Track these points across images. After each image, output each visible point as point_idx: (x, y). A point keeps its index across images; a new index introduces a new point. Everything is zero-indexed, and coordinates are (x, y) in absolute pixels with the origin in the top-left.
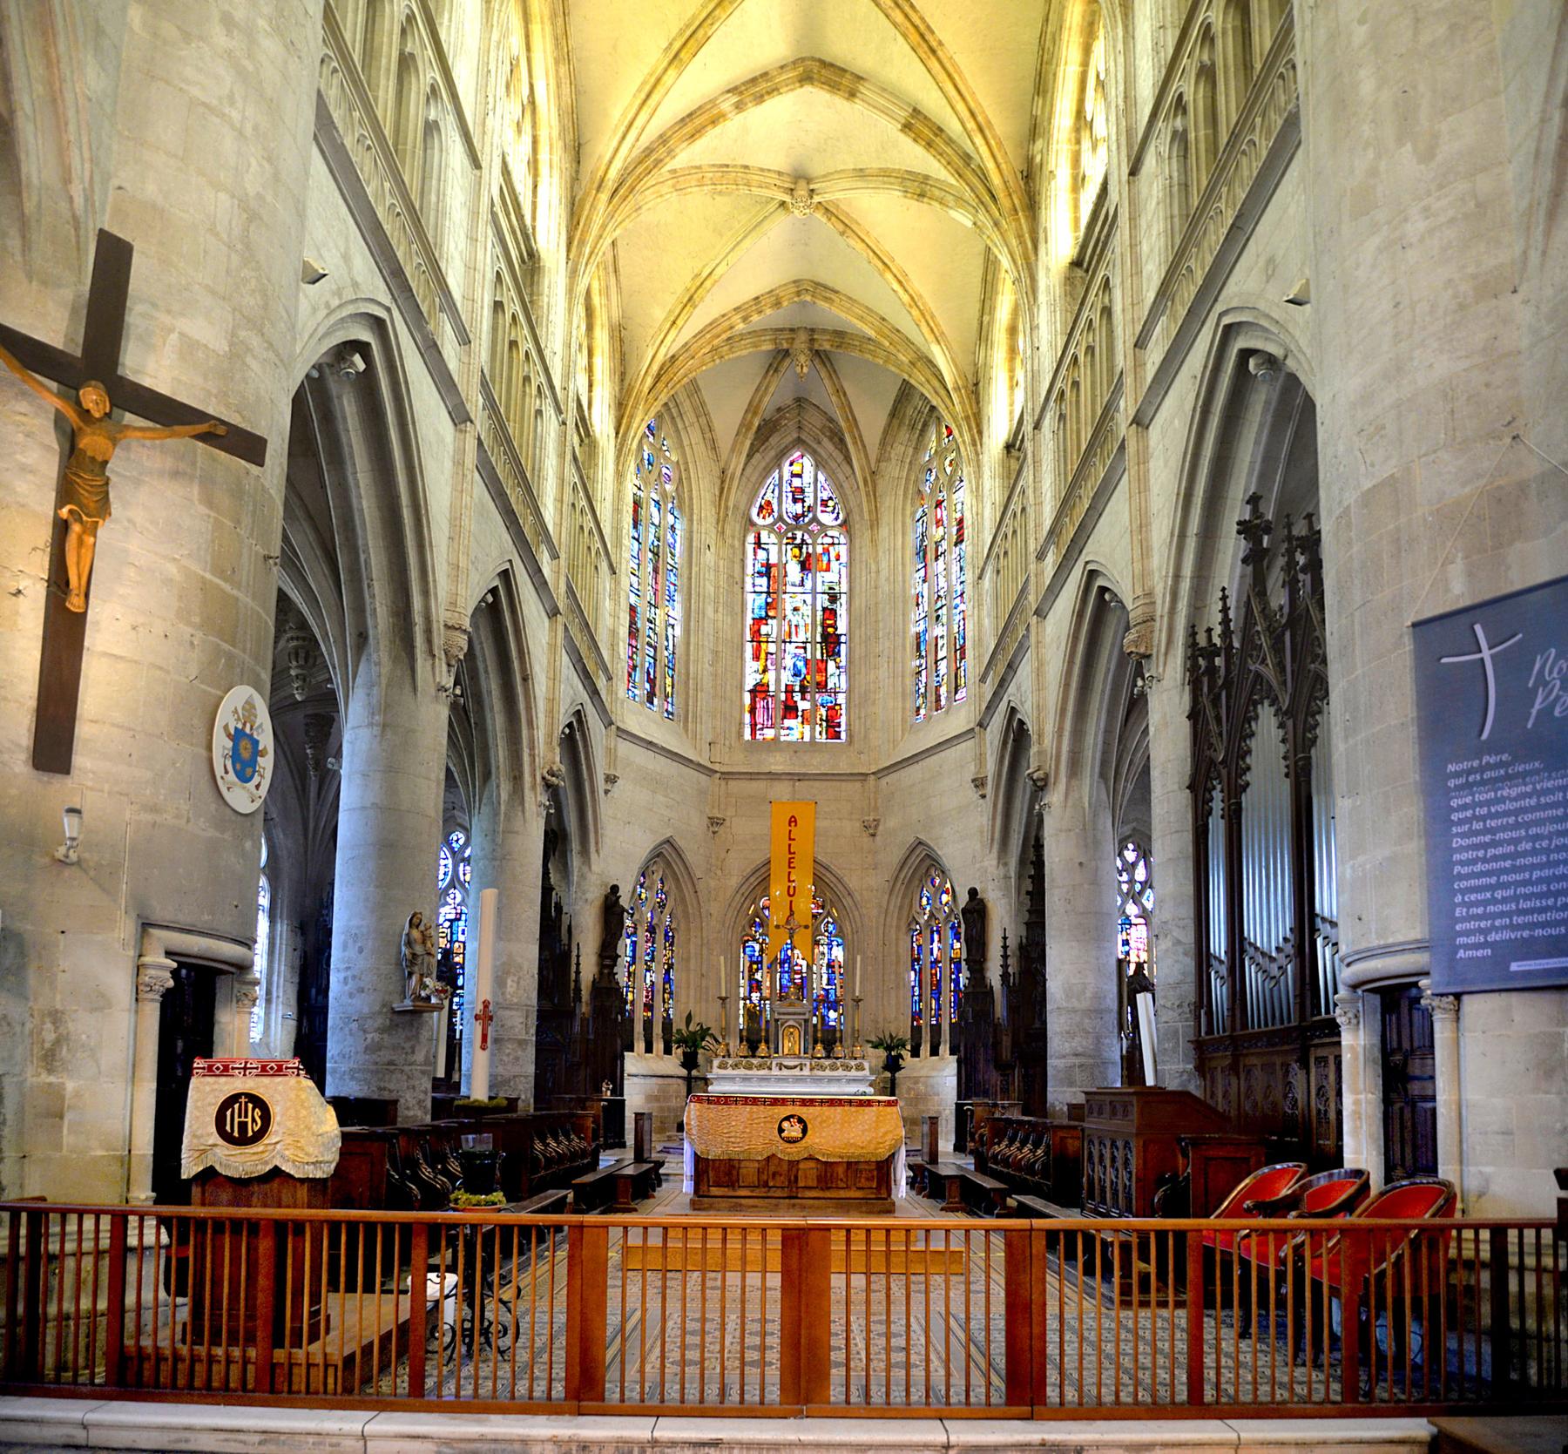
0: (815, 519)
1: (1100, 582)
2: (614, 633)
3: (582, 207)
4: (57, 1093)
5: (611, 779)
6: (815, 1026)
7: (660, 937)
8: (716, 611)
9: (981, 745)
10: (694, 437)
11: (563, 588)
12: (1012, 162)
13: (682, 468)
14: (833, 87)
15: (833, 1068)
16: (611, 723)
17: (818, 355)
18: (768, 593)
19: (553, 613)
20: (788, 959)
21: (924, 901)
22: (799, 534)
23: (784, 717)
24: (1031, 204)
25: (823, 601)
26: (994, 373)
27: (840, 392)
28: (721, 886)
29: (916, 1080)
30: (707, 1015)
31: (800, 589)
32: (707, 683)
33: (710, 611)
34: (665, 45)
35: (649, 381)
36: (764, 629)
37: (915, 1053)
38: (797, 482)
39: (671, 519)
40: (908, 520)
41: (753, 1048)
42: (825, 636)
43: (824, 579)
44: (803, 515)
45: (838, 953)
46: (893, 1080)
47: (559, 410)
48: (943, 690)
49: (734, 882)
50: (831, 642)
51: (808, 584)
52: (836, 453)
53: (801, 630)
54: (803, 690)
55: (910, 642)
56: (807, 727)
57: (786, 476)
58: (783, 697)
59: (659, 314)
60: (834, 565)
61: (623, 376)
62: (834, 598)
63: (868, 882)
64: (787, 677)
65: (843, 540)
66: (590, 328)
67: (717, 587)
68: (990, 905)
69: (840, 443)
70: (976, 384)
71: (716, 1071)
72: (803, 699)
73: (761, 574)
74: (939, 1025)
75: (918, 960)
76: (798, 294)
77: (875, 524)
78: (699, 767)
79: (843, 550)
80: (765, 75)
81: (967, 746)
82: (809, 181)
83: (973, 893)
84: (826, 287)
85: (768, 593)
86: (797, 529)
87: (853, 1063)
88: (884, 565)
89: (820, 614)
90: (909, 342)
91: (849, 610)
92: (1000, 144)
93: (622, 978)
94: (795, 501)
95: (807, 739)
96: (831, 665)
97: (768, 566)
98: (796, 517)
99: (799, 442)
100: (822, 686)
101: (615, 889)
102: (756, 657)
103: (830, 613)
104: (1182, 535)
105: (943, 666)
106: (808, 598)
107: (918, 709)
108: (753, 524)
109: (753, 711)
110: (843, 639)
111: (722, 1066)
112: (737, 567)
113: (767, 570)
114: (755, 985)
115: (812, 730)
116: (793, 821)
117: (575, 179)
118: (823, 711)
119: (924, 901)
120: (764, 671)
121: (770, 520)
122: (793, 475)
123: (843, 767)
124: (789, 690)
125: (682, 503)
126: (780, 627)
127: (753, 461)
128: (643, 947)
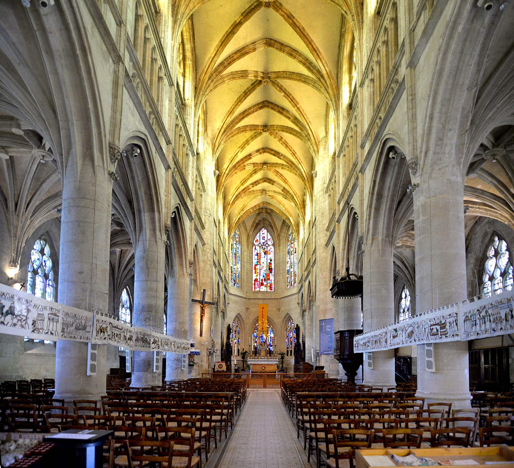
1: (354, 211)
2: (228, 274)
5: (228, 304)
7: (237, 332)
9: (299, 296)
11: (194, 210)
12: (301, 199)
14: (269, 183)
17: (267, 212)
19: (168, 168)
20: (262, 336)
24: (304, 207)
25: (269, 261)
27: (272, 219)
28: (249, 322)
29: (287, 361)
30: (246, 349)
32: (245, 280)
36: (257, 267)
37: (287, 355)
38: (263, 235)
41: (256, 355)
42: (269, 269)
43: (269, 256)
45: (272, 335)
46: (283, 361)
49: (251, 321)
50: (270, 269)
54: (265, 280)
55: (286, 271)
59: (236, 212)
61: (229, 223)
62: (271, 260)
63: (278, 321)
64: (262, 277)
66: (198, 129)
71: (249, 360)
77: (279, 246)
78: (244, 298)
79: (273, 249)
81: (296, 296)
82: (265, 191)
83: (297, 325)
86: (263, 245)
88: (281, 254)
90: (285, 215)
93: (231, 342)
96: (271, 274)
97: (257, 254)
99: (264, 227)
100: (269, 279)
101: (229, 325)
103: (270, 263)
104: (373, 194)
105: (293, 277)
109: (255, 284)
113: (257, 254)
116: (263, 308)
117: (224, 202)
118: (269, 285)
121: (258, 243)
123: (273, 297)
124: (262, 280)
125: (240, 242)
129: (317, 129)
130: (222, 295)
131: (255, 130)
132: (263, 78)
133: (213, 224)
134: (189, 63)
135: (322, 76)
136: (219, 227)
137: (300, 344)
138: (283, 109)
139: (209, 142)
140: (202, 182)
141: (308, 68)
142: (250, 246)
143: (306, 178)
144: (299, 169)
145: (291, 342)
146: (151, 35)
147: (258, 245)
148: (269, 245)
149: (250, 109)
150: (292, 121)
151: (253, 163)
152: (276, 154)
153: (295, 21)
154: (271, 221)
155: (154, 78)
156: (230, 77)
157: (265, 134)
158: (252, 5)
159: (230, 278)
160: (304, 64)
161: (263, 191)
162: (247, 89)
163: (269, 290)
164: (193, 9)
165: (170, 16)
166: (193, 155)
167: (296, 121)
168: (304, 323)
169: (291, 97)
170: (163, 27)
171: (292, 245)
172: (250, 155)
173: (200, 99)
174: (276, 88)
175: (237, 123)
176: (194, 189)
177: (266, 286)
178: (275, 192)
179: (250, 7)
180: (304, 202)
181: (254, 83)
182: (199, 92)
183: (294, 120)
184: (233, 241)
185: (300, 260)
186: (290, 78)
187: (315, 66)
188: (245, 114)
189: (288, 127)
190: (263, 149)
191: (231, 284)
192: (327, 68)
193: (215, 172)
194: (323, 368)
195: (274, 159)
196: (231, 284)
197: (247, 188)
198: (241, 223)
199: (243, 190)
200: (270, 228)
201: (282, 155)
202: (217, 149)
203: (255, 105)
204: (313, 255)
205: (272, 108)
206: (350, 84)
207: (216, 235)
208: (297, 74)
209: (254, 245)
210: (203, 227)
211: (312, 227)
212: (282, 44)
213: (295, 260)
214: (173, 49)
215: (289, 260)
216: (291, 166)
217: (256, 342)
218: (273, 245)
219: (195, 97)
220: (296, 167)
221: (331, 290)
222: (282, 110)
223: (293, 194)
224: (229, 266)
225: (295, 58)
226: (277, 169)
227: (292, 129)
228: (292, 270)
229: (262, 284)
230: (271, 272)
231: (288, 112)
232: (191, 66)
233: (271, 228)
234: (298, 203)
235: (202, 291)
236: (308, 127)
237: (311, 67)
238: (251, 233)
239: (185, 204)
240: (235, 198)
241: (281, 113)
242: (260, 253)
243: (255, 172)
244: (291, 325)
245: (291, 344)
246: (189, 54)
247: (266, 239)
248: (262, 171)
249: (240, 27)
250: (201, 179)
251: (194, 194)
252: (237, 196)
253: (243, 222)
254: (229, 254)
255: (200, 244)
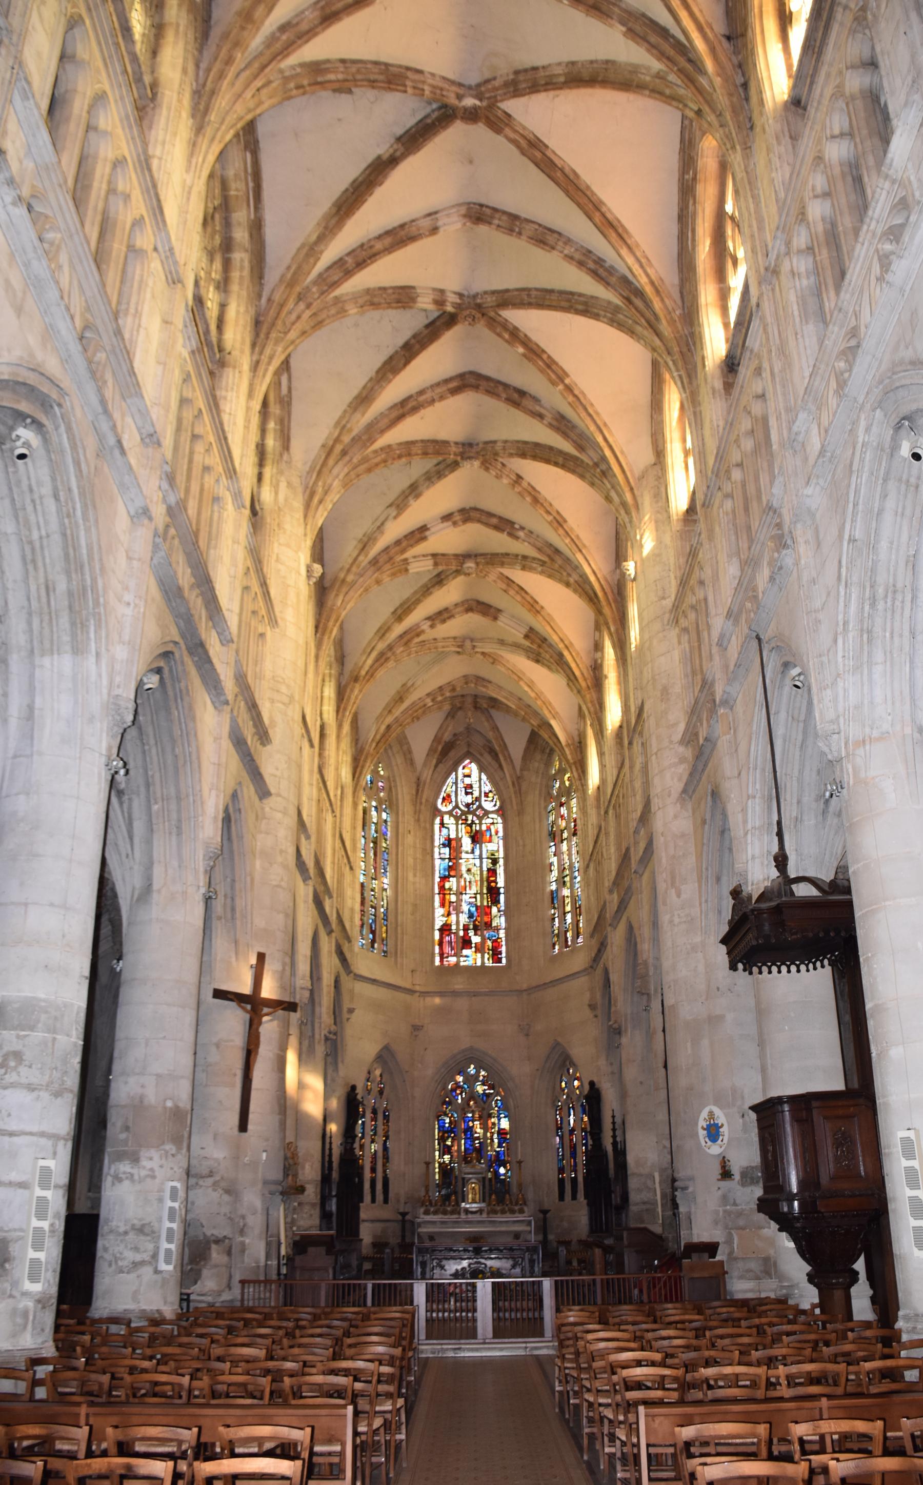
0: (480, 807)
2: (352, 910)
3: (345, 690)
4: (243, 1244)
5: (351, 1011)
6: (490, 1180)
7: (380, 1117)
8: (415, 875)
10: (399, 760)
13: (390, 780)
15: (503, 1212)
16: (351, 972)
17: (476, 707)
18: (450, 859)
21: (563, 1084)
22: (470, 817)
23: (463, 948)
25: (487, 864)
26: (605, 671)
27: (495, 728)
31: (471, 856)
33: (411, 875)
34: (392, 610)
35: (374, 745)
36: (447, 885)
38: (467, 781)
39: (384, 816)
40: (543, 813)
43: (488, 847)
44: (473, 804)
45: (505, 1124)
47: (333, 812)
48: (569, 935)
49: (430, 1072)
50: (493, 893)
51: (477, 852)
52: (494, 763)
53: (474, 884)
54: (476, 929)
56: (479, 955)
57: (460, 776)
58: (461, 933)
60: (495, 838)
63: (521, 1071)
65: (500, 820)
67: (415, 859)
68: (603, 1093)
69: (495, 757)
70: (580, 743)
72: (476, 934)
73: (444, 845)
74: (576, 1177)
75: (561, 1128)
76: (466, 683)
77: (521, 812)
79: (500, 827)
80: (446, 609)
82: (472, 640)
83: (592, 1084)
84: (483, 679)
85: (450, 859)
86: (469, 814)
87: (516, 1208)
89: (485, 873)
91: (505, 870)
92: (578, 654)
94: (467, 793)
95: (479, 963)
96: (494, 910)
97: (449, 840)
98: (468, 805)
99: (469, 755)
100: (488, 925)
101: (353, 1088)
102: (442, 905)
103: (492, 872)
105: (569, 918)
106: (477, 862)
107: (554, 945)
108: (439, 811)
110: (502, 890)
111: (427, 1213)
112: (428, 842)
113: (448, 843)
114: (446, 1150)
115: (483, 957)
118: (489, 943)
119: (563, 1084)
120: (449, 914)
121: (450, 807)
122: (465, 776)
124: (466, 928)
125: (391, 804)
126: (458, 882)
127: (439, 769)
128: (369, 1124)
129: (625, 443)
130: (327, 979)
131: (438, 453)
132: (458, 306)
133: (299, 729)
134: (241, 257)
135: (639, 293)
136: (341, 815)
137: (605, 1154)
138: (522, 393)
139: (296, 481)
140: (267, 594)
141: (594, 274)
142: (425, 814)
143: (600, 594)
144: (577, 568)
145: (573, 1148)
146: (194, 390)
147: (450, 813)
148: (487, 813)
149: (421, 392)
150: (550, 426)
151: (434, 555)
152: (504, 525)
153: (549, 153)
154: (491, 735)
155: (116, 246)
156: (361, 301)
157: (470, 470)
158: (426, 117)
159: (358, 922)
160: (581, 264)
161: (463, 644)
162: (414, 336)
163: (489, 963)
164: (255, 109)
165: (185, 114)
166: (240, 506)
167: (562, 424)
168: (618, 1075)
169: (545, 356)
170: (161, 133)
171: (563, 811)
172: (423, 529)
173: (268, 351)
174: (499, 335)
175: (382, 432)
176: (236, 608)
177: (479, 949)
178: (502, 642)
179: (421, 121)
180: (597, 669)
181: (432, 323)
182: (268, 334)
183: (555, 423)
184: (370, 798)
185: (592, 858)
186: (540, 306)
187: (612, 267)
188: (407, 407)
189: (537, 445)
190: (462, 511)
191: (360, 942)
192: (649, 271)
193: (309, 570)
194: (711, 1248)
195: (499, 542)
196: (360, 942)
197: (414, 632)
198: (393, 742)
199: (401, 637)
200: (487, 758)
201: (522, 528)
202: (320, 502)
203: (438, 384)
204: (636, 832)
205: (489, 392)
206: (724, 310)
207: (311, 772)
208: (561, 293)
209: (437, 812)
210: (264, 737)
211: (630, 743)
212: (514, 217)
213: (574, 857)
214: (189, 193)
215: (554, 860)
216: (556, 562)
217: (446, 1150)
218: (501, 811)
219: (253, 345)
220: (568, 560)
221: (724, 941)
222: (517, 397)
223: (561, 646)
224: (353, 882)
225: (553, 248)
226: (507, 572)
227: (551, 448)
228: (566, 892)
229: (466, 943)
230: (496, 902)
231: (536, 400)
232: (246, 264)
233: (491, 757)
234: (577, 673)
235: (253, 961)
236: (600, 439)
237: (601, 271)
238: (427, 775)
239: (198, 650)
240: (377, 660)
241: (516, 404)
242: (458, 840)
243: (439, 580)
244: (569, 1084)
245: (574, 1154)
246: (241, 235)
247: (476, 794)
248: (461, 579)
249: (393, 169)
250: (264, 584)
251: (233, 621)
252: (382, 654)
253: (403, 741)
254: (354, 841)
255: (249, 791)
